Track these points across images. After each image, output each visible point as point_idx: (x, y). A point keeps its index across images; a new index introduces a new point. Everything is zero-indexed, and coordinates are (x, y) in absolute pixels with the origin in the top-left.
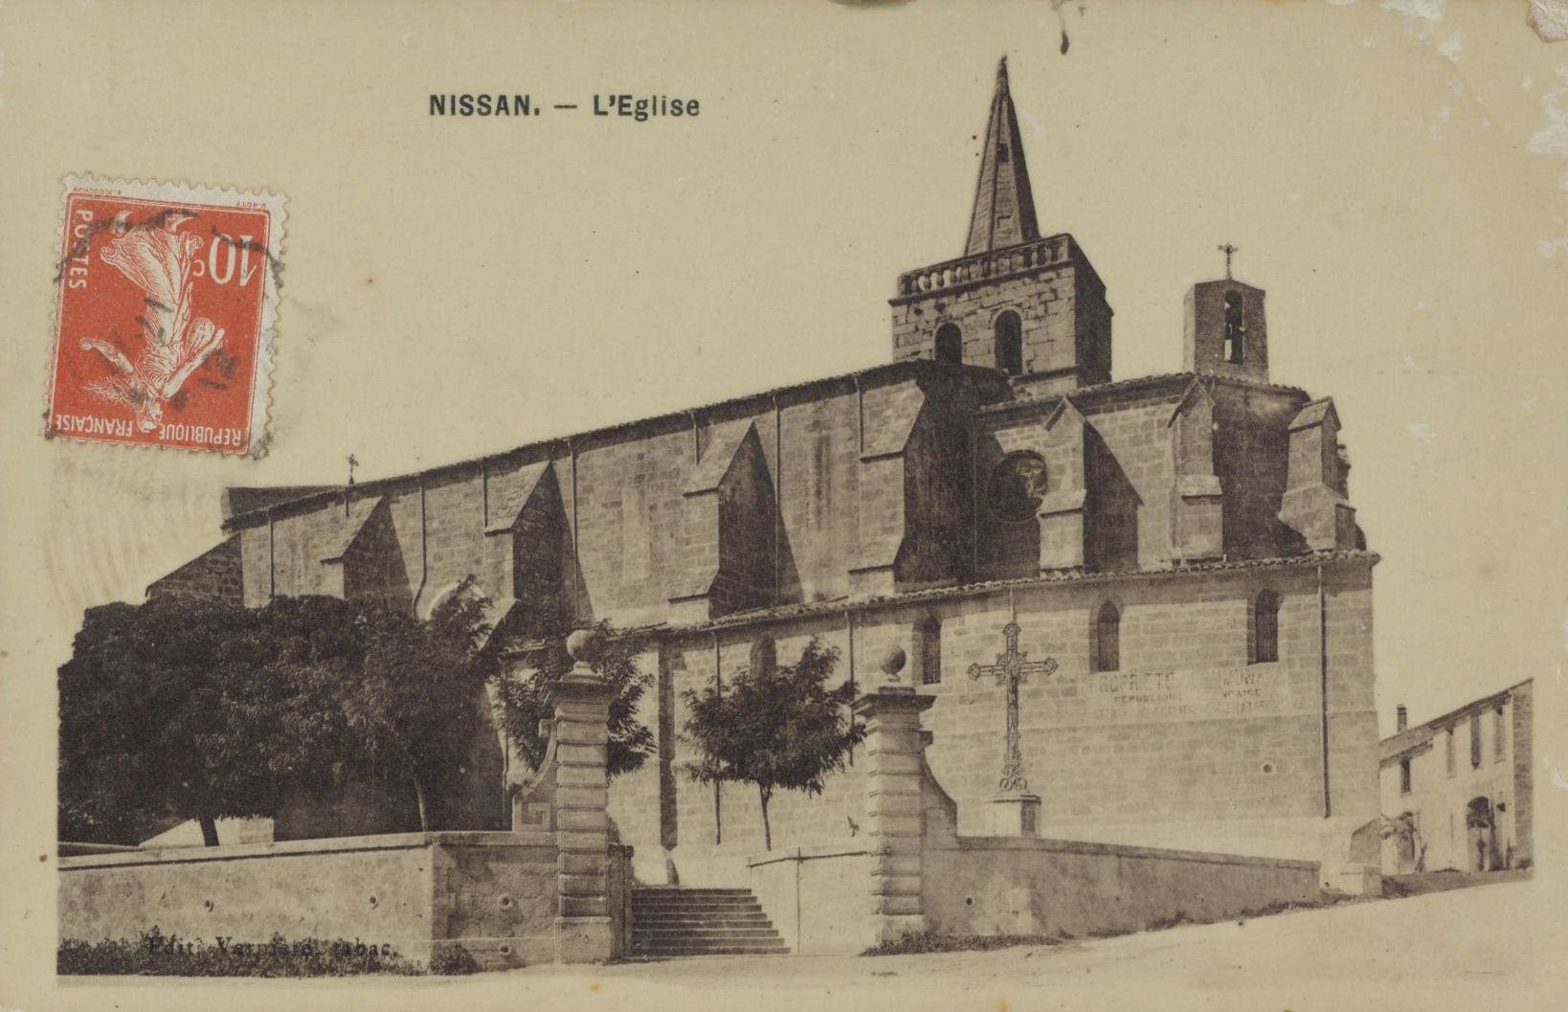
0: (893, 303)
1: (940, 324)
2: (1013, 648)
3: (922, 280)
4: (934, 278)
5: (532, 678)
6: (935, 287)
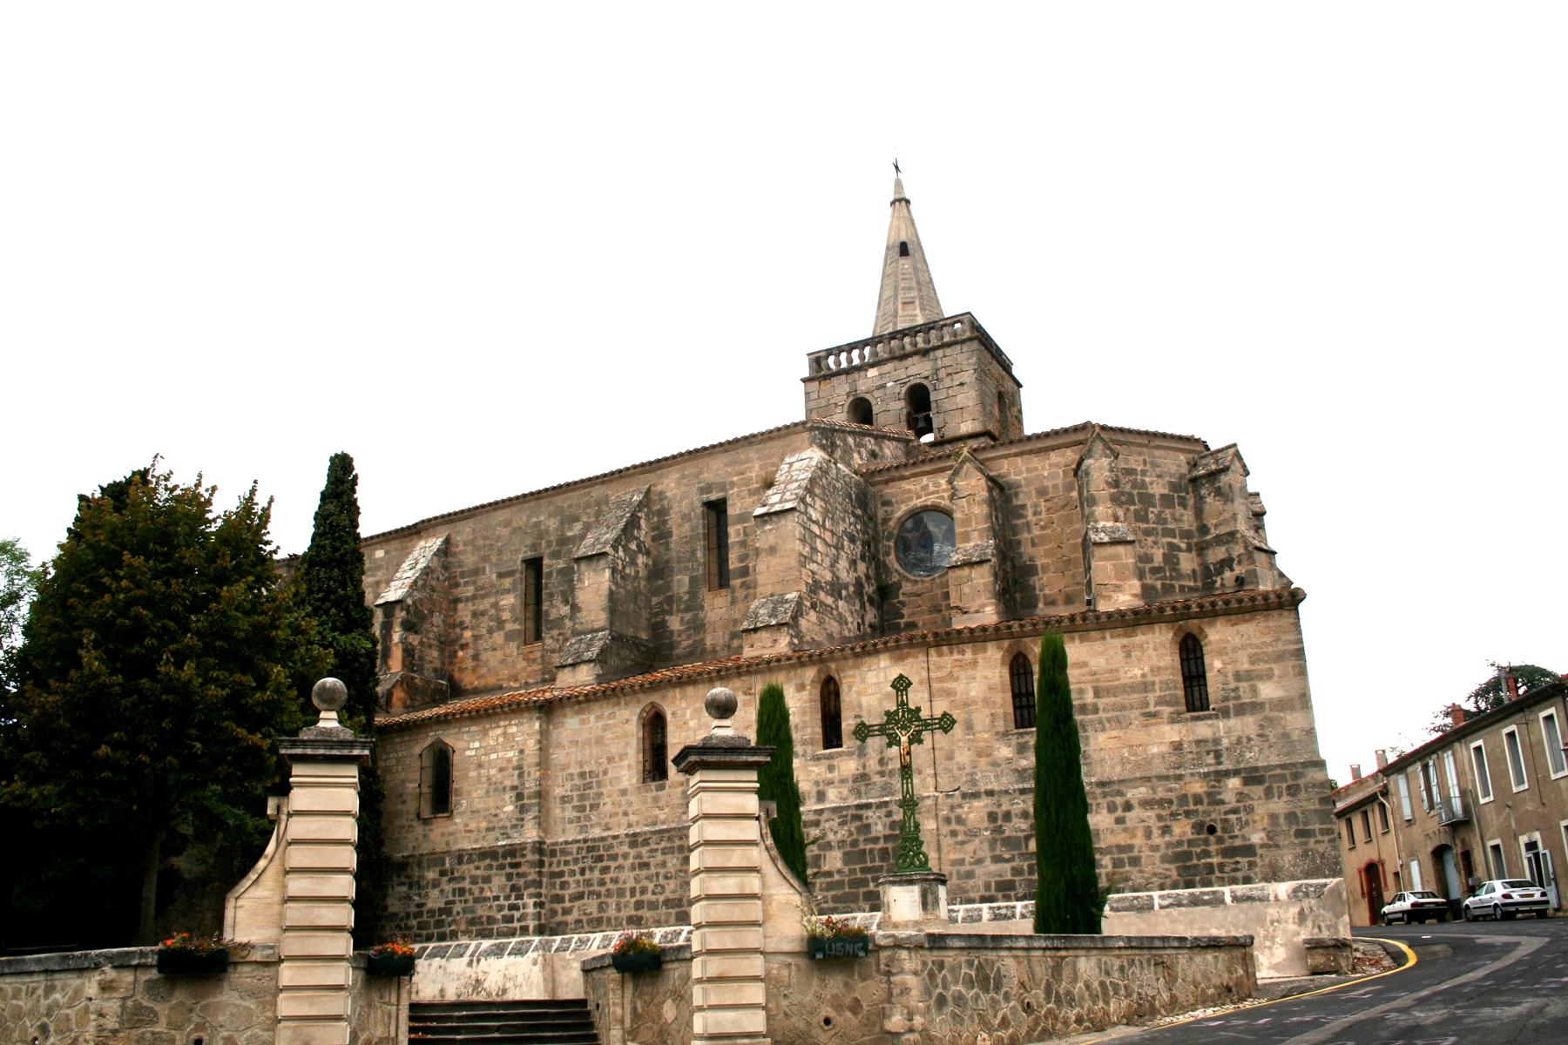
0: (804, 381)
1: (851, 398)
2: (927, 725)
3: (831, 359)
4: (843, 356)
5: (209, 502)
6: (844, 365)
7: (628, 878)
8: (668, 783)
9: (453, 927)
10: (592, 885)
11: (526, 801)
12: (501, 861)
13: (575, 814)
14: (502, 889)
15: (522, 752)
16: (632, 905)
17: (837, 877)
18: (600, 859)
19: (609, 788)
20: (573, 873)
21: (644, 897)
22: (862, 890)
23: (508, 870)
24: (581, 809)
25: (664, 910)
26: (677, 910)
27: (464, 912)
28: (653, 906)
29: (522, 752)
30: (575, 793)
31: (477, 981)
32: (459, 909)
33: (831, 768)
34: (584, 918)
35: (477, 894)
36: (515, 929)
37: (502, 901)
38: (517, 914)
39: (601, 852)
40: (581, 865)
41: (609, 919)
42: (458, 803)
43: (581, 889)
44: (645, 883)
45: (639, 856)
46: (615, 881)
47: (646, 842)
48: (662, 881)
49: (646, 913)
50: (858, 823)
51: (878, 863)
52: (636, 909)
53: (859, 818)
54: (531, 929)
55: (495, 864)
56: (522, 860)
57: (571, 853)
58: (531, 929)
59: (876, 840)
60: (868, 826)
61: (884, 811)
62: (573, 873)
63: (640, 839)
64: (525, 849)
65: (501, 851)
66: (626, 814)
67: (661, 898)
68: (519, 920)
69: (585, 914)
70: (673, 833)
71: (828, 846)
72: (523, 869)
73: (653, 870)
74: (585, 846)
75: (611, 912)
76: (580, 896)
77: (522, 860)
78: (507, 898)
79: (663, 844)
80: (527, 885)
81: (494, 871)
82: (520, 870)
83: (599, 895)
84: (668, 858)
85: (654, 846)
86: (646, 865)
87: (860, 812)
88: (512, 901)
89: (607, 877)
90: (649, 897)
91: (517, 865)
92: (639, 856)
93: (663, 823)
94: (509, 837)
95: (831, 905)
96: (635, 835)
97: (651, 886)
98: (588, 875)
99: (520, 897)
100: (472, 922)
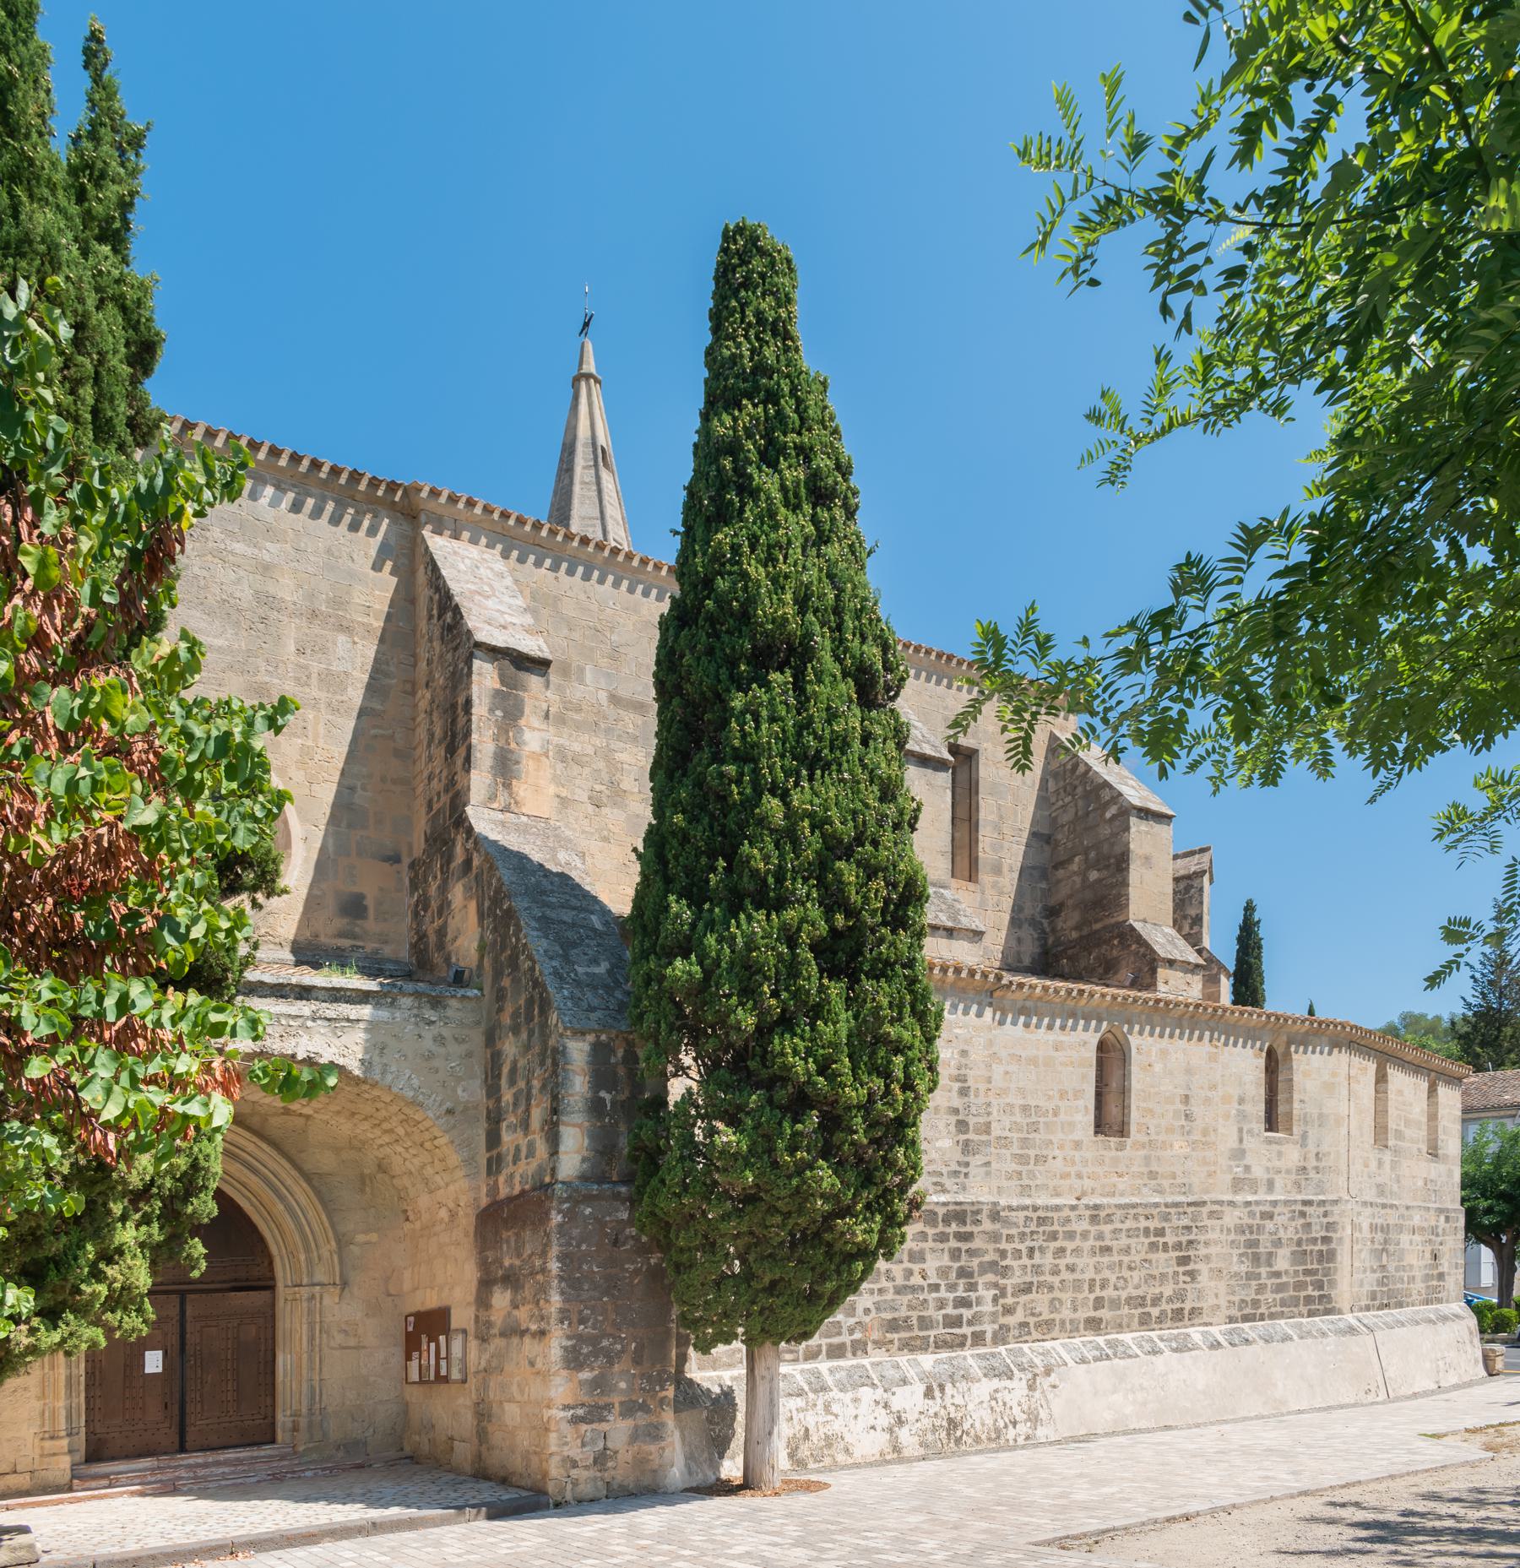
7: (1086, 1262)
8: (1129, 1141)
9: (857, 1335)
10: (1042, 1273)
11: (971, 1136)
12: (941, 1228)
13: (1015, 1167)
14: (943, 1272)
15: (964, 1053)
16: (1091, 1304)
17: (1284, 1279)
18: (1053, 1236)
19: (1060, 1135)
20: (1017, 1254)
21: (1104, 1294)
22: (1303, 1294)
23: (953, 1244)
24: (1022, 1159)
25: (1125, 1310)
26: (1140, 1310)
27: (878, 1309)
28: (1115, 1304)
29: (964, 1053)
30: (1015, 1135)
31: (950, 1421)
32: (869, 1305)
33: (1280, 1154)
34: (1032, 1320)
35: (900, 1281)
36: (964, 1336)
37: (943, 1293)
38: (967, 1313)
39: (1056, 1227)
40: (1029, 1243)
41: (1063, 1322)
42: (586, 1086)
43: (1028, 1279)
44: (1106, 1274)
45: (1100, 1237)
46: (1071, 1268)
47: (1109, 1219)
48: (1126, 1273)
49: (1105, 1314)
50: (1302, 1221)
51: (1315, 1266)
52: (1096, 1309)
53: (1303, 1214)
54: (989, 1336)
55: (931, 1231)
56: (975, 1229)
57: (1016, 1225)
58: (989, 1336)
59: (1314, 1241)
60: (1309, 1224)
61: (1322, 1210)
62: (1017, 1254)
63: (1103, 1214)
64: (978, 1212)
65: (941, 1211)
66: (1079, 1176)
67: (1124, 1295)
68: (970, 1323)
69: (1033, 1314)
70: (1140, 1210)
71: (1278, 1243)
72: (977, 1243)
73: (1116, 1258)
74: (1034, 1215)
75: (1066, 1313)
76: (1027, 1289)
77: (975, 1229)
78: (952, 1287)
79: (1129, 1224)
80: (983, 1271)
81: (930, 1244)
82: (973, 1245)
83: (1051, 1288)
84: (1132, 1241)
85: (1119, 1226)
86: (1108, 1249)
87: (1305, 1209)
88: (960, 1293)
89: (1062, 1263)
90: (1109, 1293)
91: (966, 1237)
92: (1100, 1237)
93: (1122, 1195)
94: (944, 1191)
95: (1279, 1309)
96: (1096, 1207)
97: (1113, 1279)
98: (1037, 1259)
99: (972, 1287)
100: (893, 1325)
